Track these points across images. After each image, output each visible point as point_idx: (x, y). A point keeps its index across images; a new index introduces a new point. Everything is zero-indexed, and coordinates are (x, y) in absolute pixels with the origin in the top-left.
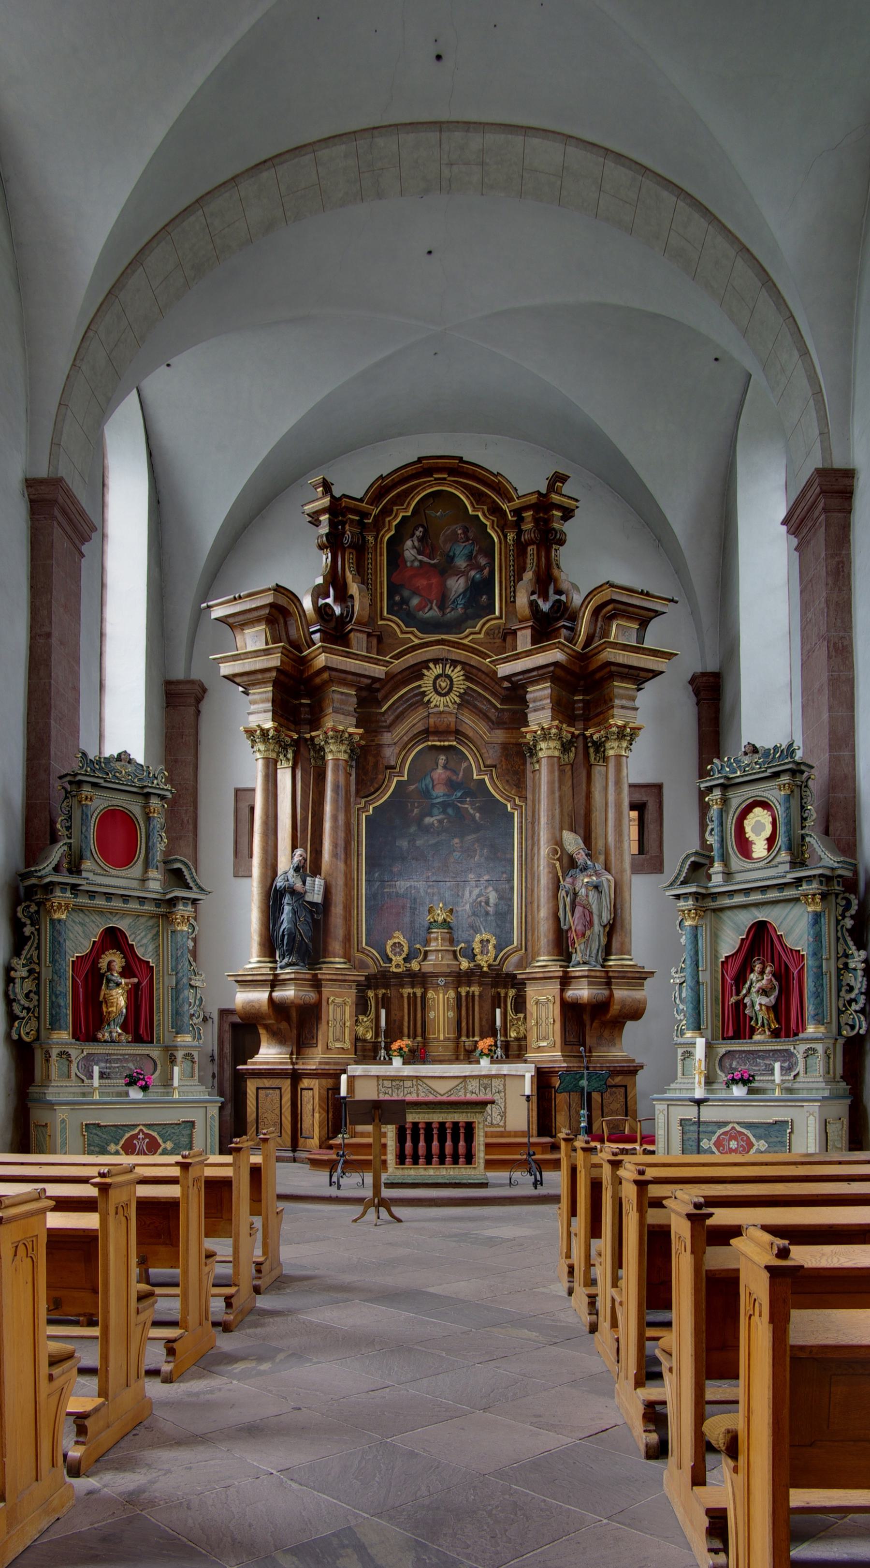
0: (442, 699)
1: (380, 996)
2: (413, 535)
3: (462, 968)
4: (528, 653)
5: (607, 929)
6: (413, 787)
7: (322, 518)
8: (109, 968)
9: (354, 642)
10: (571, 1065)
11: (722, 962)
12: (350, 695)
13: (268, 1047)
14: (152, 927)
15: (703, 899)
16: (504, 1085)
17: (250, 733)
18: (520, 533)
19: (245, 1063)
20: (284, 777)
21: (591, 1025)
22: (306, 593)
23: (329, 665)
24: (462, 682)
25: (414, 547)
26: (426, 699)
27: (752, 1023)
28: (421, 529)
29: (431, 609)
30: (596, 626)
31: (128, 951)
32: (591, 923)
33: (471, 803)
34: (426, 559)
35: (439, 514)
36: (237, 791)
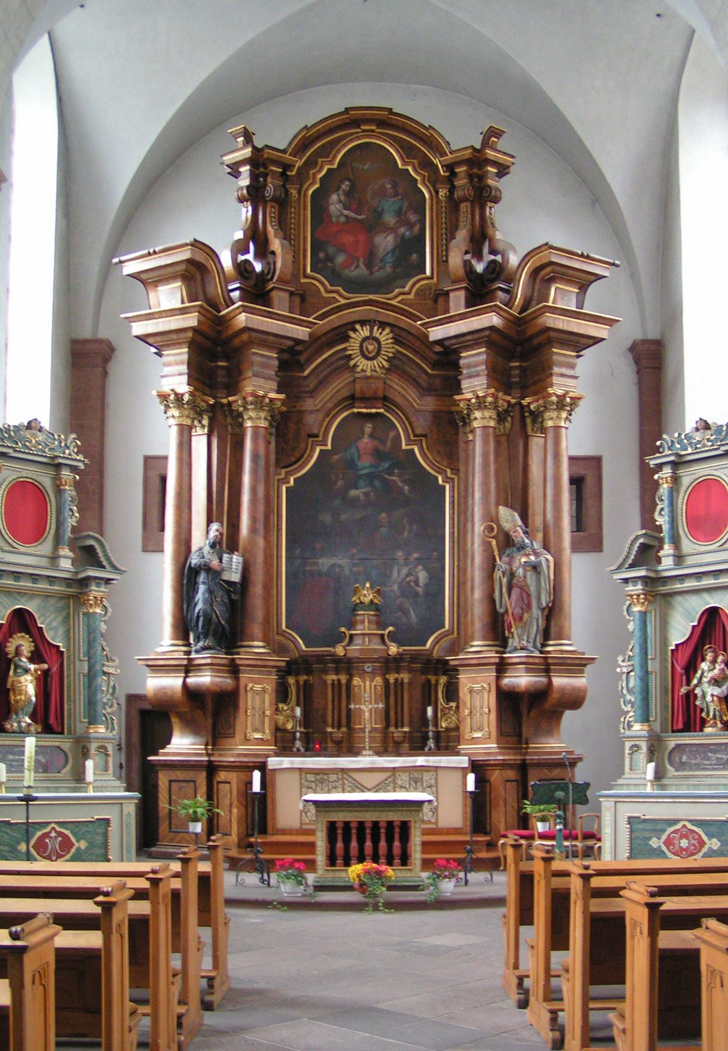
0: (369, 363)
1: (301, 683)
2: (339, 188)
3: (390, 653)
4: (462, 317)
5: (546, 613)
6: (336, 457)
7: (242, 169)
8: (18, 653)
9: (276, 302)
10: (507, 758)
11: (672, 650)
12: (270, 357)
13: (181, 737)
14: (63, 608)
15: (652, 583)
16: (436, 779)
17: (163, 397)
18: (452, 189)
19: (157, 754)
20: (199, 444)
21: (528, 714)
22: (225, 248)
23: (250, 326)
24: (391, 346)
25: (340, 201)
26: (352, 363)
27: (704, 715)
28: (347, 183)
29: (357, 267)
30: (533, 288)
31: (37, 635)
32: (529, 606)
33: (400, 475)
34: (352, 215)
35: (365, 167)
36: (147, 459)
